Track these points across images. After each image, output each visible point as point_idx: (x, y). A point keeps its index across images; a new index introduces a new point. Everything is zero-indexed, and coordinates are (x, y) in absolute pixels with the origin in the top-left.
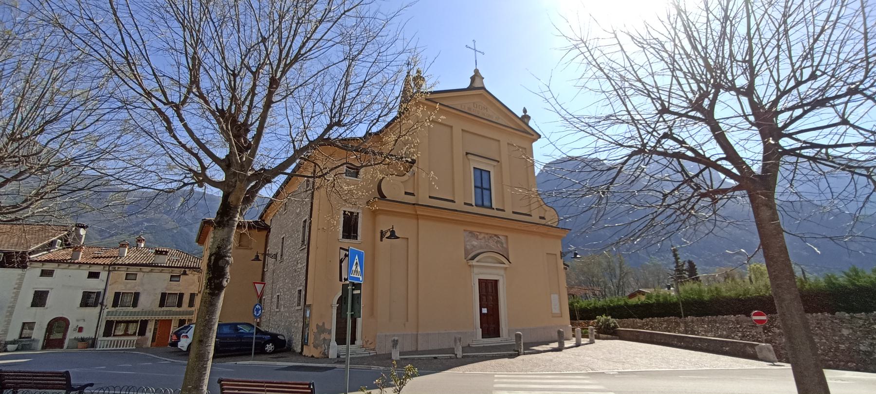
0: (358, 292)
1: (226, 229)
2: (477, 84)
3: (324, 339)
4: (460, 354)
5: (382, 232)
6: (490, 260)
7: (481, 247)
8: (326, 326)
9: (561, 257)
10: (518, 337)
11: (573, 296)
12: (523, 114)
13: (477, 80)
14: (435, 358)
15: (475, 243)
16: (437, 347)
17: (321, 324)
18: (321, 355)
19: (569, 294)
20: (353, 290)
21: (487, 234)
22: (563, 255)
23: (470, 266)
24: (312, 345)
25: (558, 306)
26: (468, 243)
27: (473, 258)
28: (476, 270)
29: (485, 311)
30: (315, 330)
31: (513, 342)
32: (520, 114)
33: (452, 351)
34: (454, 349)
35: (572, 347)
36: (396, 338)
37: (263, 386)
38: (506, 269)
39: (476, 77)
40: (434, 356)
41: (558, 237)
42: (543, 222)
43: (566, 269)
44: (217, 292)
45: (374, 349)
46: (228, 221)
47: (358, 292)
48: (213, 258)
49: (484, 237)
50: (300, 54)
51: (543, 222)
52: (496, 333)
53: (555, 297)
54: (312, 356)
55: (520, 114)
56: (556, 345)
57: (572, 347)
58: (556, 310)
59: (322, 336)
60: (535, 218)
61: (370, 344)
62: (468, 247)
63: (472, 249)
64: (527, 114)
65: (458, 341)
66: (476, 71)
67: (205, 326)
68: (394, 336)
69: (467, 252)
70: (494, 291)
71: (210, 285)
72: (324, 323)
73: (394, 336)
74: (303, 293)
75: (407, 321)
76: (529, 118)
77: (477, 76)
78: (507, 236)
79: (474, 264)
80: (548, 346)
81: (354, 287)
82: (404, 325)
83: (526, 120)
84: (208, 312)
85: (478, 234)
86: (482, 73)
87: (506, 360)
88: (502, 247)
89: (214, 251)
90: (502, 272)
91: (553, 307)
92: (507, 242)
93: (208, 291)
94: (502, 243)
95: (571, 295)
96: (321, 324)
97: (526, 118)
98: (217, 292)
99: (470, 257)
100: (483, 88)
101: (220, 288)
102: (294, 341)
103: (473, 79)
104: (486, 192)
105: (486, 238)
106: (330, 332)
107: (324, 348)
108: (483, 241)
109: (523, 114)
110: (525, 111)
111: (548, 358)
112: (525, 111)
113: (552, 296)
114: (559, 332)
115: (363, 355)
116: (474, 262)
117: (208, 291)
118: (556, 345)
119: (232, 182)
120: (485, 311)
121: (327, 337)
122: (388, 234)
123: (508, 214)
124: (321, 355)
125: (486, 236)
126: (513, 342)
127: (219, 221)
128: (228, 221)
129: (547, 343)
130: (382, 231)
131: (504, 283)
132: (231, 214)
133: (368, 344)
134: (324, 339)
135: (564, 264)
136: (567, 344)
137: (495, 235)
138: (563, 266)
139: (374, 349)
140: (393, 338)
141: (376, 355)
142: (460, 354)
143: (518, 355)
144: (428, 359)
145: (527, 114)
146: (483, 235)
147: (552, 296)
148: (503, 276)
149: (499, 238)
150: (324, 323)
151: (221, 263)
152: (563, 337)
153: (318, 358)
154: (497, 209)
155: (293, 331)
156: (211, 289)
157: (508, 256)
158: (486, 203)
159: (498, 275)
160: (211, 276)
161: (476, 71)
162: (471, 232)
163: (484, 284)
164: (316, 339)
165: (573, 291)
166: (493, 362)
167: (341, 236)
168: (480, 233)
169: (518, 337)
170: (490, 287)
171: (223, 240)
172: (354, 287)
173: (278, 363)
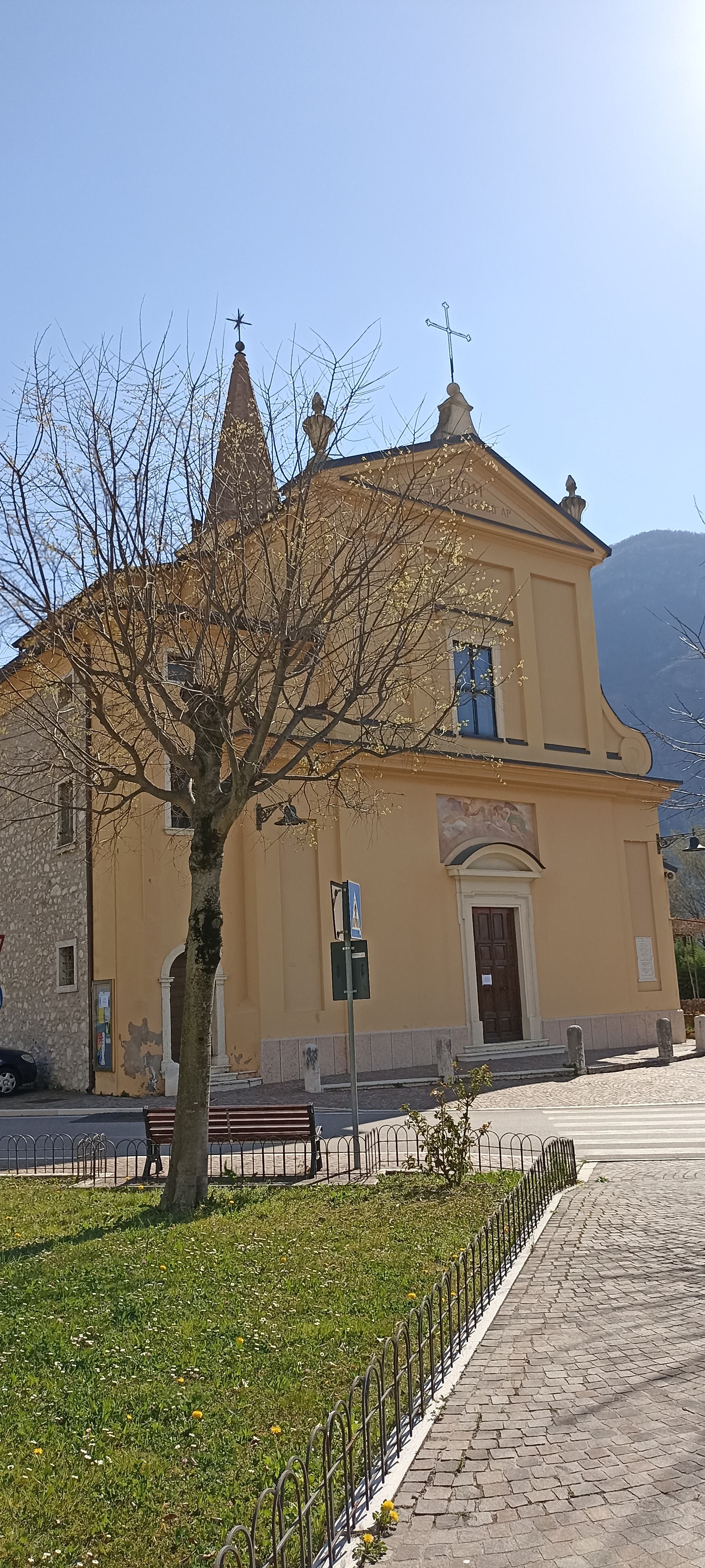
0: (361, 955)
1: (214, 872)
2: (456, 427)
3: (149, 1055)
4: (449, 1075)
5: (259, 809)
6: (496, 862)
7: (475, 834)
8: (152, 1028)
9: (659, 848)
10: (574, 1036)
11: (684, 939)
12: (567, 494)
13: (457, 413)
14: (398, 1086)
15: (461, 824)
16: (388, 1066)
17: (139, 1023)
18: (144, 1091)
19: (676, 936)
20: (353, 952)
21: (488, 801)
22: (662, 843)
23: (453, 877)
24: (120, 1071)
25: (652, 965)
26: (446, 825)
27: (459, 860)
28: (466, 888)
29: (487, 980)
30: (127, 1037)
31: (562, 1047)
32: (558, 494)
33: (432, 1070)
34: (436, 1065)
35: (689, 1057)
36: (313, 1046)
37: (224, 1117)
38: (532, 881)
39: (453, 406)
40: (395, 1082)
41: (655, 803)
42: (614, 765)
43: (668, 876)
44: (212, 967)
45: (255, 1074)
46: (215, 859)
47: (361, 955)
48: (201, 917)
49: (482, 810)
50: (365, 633)
51: (614, 765)
52: (515, 1031)
53: (644, 944)
54: (125, 1095)
55: (558, 494)
56: (654, 1053)
57: (689, 1057)
58: (647, 974)
59: (144, 1049)
60: (597, 759)
61: (246, 1062)
62: (446, 833)
63: (455, 838)
64: (577, 493)
65: (444, 1048)
66: (454, 389)
67: (203, 1018)
68: (308, 1041)
69: (445, 846)
70: (506, 934)
71: (203, 957)
72: (145, 1021)
73: (308, 1041)
74: (80, 955)
75: (323, 1009)
76: (582, 503)
77: (458, 403)
78: (533, 805)
79: (462, 873)
80: (635, 1056)
81: (353, 948)
82: (317, 1017)
83: (573, 511)
84: (204, 997)
85: (468, 802)
86: (468, 394)
87: (552, 1085)
88: (523, 830)
89: (200, 906)
90: (524, 890)
91: (640, 966)
92: (534, 820)
93: (201, 966)
94: (522, 822)
95: (681, 938)
96: (139, 1023)
97: (574, 503)
98: (212, 967)
99: (452, 856)
100: (475, 438)
101: (215, 959)
102: (56, 1067)
103: (445, 410)
104: (483, 701)
105: (486, 811)
106: (159, 1041)
107: (149, 1076)
108: (479, 818)
109: (567, 494)
110: (571, 485)
111: (641, 1078)
112: (571, 485)
113: (638, 940)
114: (661, 1024)
115: (236, 1087)
116: (462, 870)
117: (201, 966)
118: (654, 1053)
119: (210, 796)
120: (487, 980)
121: (154, 1049)
122: (279, 814)
123: (535, 752)
124: (144, 1091)
125: (487, 807)
126: (562, 1047)
127: (203, 860)
128: (215, 859)
129: (632, 1051)
130: (259, 805)
131: (528, 916)
132: (218, 849)
133: (242, 1061)
134: (149, 1055)
135: (666, 865)
136: (678, 1051)
137: (507, 803)
138: (662, 870)
139: (255, 1074)
140: (307, 1046)
141: (263, 1086)
142: (449, 1075)
143: (576, 1075)
144: (383, 1088)
145: (577, 493)
146: (478, 805)
147: (638, 940)
148: (526, 898)
149: (516, 810)
150: (145, 1021)
151: (214, 922)
152: (669, 1035)
153: (138, 1097)
154: (508, 740)
155: (50, 1042)
156: (205, 963)
157: (537, 851)
158: (485, 726)
159: (516, 896)
160: (202, 944)
161: (454, 389)
162: (451, 799)
163: (483, 919)
164: (128, 1056)
165: (683, 927)
166: (529, 1089)
167: (169, 823)
168: (473, 799)
169: (574, 1036)
170: (497, 921)
171: (212, 888)
172: (353, 948)
173: (62, 1111)
